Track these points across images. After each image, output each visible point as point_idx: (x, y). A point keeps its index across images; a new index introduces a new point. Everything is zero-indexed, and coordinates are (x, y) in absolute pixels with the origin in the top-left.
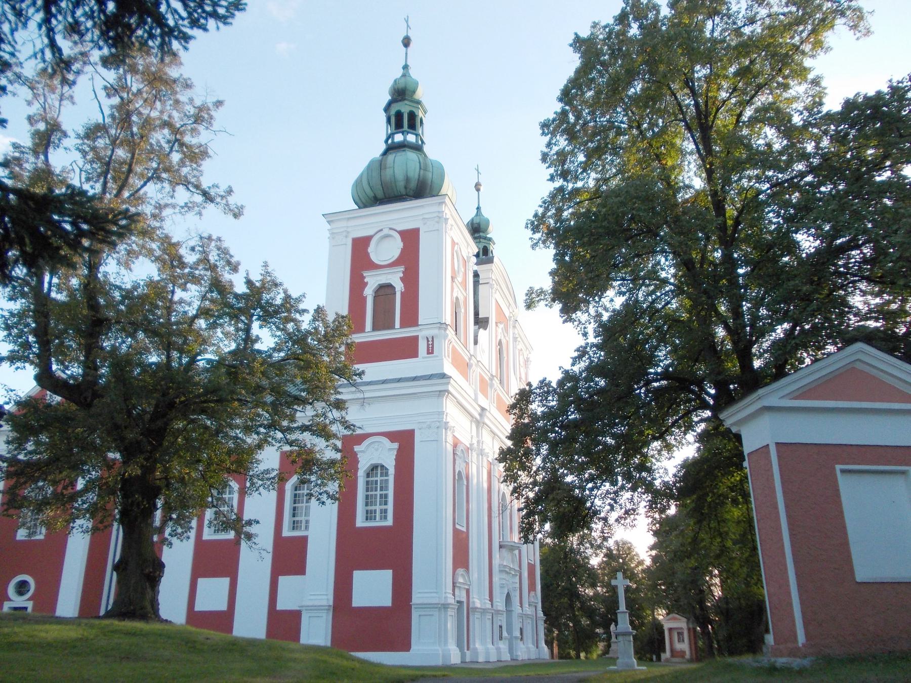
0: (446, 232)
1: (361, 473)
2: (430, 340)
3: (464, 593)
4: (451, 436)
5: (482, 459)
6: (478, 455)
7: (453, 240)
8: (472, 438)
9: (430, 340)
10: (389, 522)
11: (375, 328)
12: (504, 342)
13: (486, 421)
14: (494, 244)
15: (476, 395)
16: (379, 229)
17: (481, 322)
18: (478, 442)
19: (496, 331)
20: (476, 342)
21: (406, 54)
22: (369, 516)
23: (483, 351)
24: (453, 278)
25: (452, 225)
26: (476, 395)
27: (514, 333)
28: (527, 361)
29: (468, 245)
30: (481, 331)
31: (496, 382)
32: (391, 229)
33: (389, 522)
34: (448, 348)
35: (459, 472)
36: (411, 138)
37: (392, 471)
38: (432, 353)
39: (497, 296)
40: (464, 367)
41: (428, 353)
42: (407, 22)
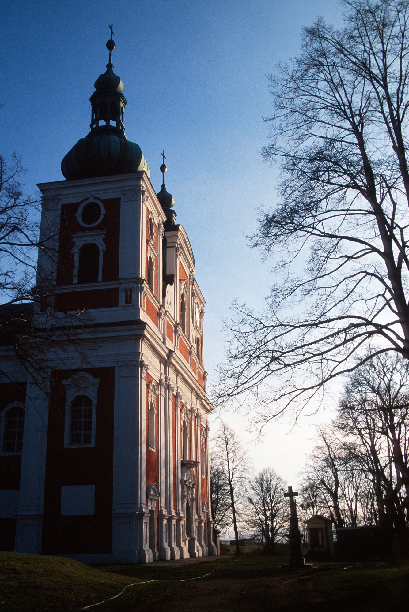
0: (143, 202)
1: (68, 403)
2: (129, 292)
3: (155, 504)
4: (145, 373)
5: (169, 392)
6: (165, 389)
7: (148, 209)
8: (161, 375)
9: (129, 292)
10: (93, 444)
11: (81, 281)
12: (185, 295)
13: (173, 360)
14: (176, 215)
15: (164, 339)
16: (84, 198)
17: (169, 279)
18: (166, 378)
19: (180, 287)
20: (164, 295)
21: (110, 55)
22: (75, 439)
23: (170, 303)
24: (148, 242)
25: (148, 197)
26: (164, 339)
27: (192, 289)
28: (202, 312)
29: (159, 214)
30: (168, 286)
31: (180, 328)
32: (96, 198)
33: (93, 444)
34: (144, 299)
35: (151, 402)
36: (113, 123)
37: (94, 402)
38: (130, 302)
39: (181, 258)
40: (157, 316)
41: (127, 302)
42: (111, 28)
